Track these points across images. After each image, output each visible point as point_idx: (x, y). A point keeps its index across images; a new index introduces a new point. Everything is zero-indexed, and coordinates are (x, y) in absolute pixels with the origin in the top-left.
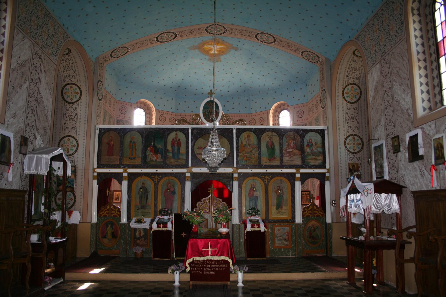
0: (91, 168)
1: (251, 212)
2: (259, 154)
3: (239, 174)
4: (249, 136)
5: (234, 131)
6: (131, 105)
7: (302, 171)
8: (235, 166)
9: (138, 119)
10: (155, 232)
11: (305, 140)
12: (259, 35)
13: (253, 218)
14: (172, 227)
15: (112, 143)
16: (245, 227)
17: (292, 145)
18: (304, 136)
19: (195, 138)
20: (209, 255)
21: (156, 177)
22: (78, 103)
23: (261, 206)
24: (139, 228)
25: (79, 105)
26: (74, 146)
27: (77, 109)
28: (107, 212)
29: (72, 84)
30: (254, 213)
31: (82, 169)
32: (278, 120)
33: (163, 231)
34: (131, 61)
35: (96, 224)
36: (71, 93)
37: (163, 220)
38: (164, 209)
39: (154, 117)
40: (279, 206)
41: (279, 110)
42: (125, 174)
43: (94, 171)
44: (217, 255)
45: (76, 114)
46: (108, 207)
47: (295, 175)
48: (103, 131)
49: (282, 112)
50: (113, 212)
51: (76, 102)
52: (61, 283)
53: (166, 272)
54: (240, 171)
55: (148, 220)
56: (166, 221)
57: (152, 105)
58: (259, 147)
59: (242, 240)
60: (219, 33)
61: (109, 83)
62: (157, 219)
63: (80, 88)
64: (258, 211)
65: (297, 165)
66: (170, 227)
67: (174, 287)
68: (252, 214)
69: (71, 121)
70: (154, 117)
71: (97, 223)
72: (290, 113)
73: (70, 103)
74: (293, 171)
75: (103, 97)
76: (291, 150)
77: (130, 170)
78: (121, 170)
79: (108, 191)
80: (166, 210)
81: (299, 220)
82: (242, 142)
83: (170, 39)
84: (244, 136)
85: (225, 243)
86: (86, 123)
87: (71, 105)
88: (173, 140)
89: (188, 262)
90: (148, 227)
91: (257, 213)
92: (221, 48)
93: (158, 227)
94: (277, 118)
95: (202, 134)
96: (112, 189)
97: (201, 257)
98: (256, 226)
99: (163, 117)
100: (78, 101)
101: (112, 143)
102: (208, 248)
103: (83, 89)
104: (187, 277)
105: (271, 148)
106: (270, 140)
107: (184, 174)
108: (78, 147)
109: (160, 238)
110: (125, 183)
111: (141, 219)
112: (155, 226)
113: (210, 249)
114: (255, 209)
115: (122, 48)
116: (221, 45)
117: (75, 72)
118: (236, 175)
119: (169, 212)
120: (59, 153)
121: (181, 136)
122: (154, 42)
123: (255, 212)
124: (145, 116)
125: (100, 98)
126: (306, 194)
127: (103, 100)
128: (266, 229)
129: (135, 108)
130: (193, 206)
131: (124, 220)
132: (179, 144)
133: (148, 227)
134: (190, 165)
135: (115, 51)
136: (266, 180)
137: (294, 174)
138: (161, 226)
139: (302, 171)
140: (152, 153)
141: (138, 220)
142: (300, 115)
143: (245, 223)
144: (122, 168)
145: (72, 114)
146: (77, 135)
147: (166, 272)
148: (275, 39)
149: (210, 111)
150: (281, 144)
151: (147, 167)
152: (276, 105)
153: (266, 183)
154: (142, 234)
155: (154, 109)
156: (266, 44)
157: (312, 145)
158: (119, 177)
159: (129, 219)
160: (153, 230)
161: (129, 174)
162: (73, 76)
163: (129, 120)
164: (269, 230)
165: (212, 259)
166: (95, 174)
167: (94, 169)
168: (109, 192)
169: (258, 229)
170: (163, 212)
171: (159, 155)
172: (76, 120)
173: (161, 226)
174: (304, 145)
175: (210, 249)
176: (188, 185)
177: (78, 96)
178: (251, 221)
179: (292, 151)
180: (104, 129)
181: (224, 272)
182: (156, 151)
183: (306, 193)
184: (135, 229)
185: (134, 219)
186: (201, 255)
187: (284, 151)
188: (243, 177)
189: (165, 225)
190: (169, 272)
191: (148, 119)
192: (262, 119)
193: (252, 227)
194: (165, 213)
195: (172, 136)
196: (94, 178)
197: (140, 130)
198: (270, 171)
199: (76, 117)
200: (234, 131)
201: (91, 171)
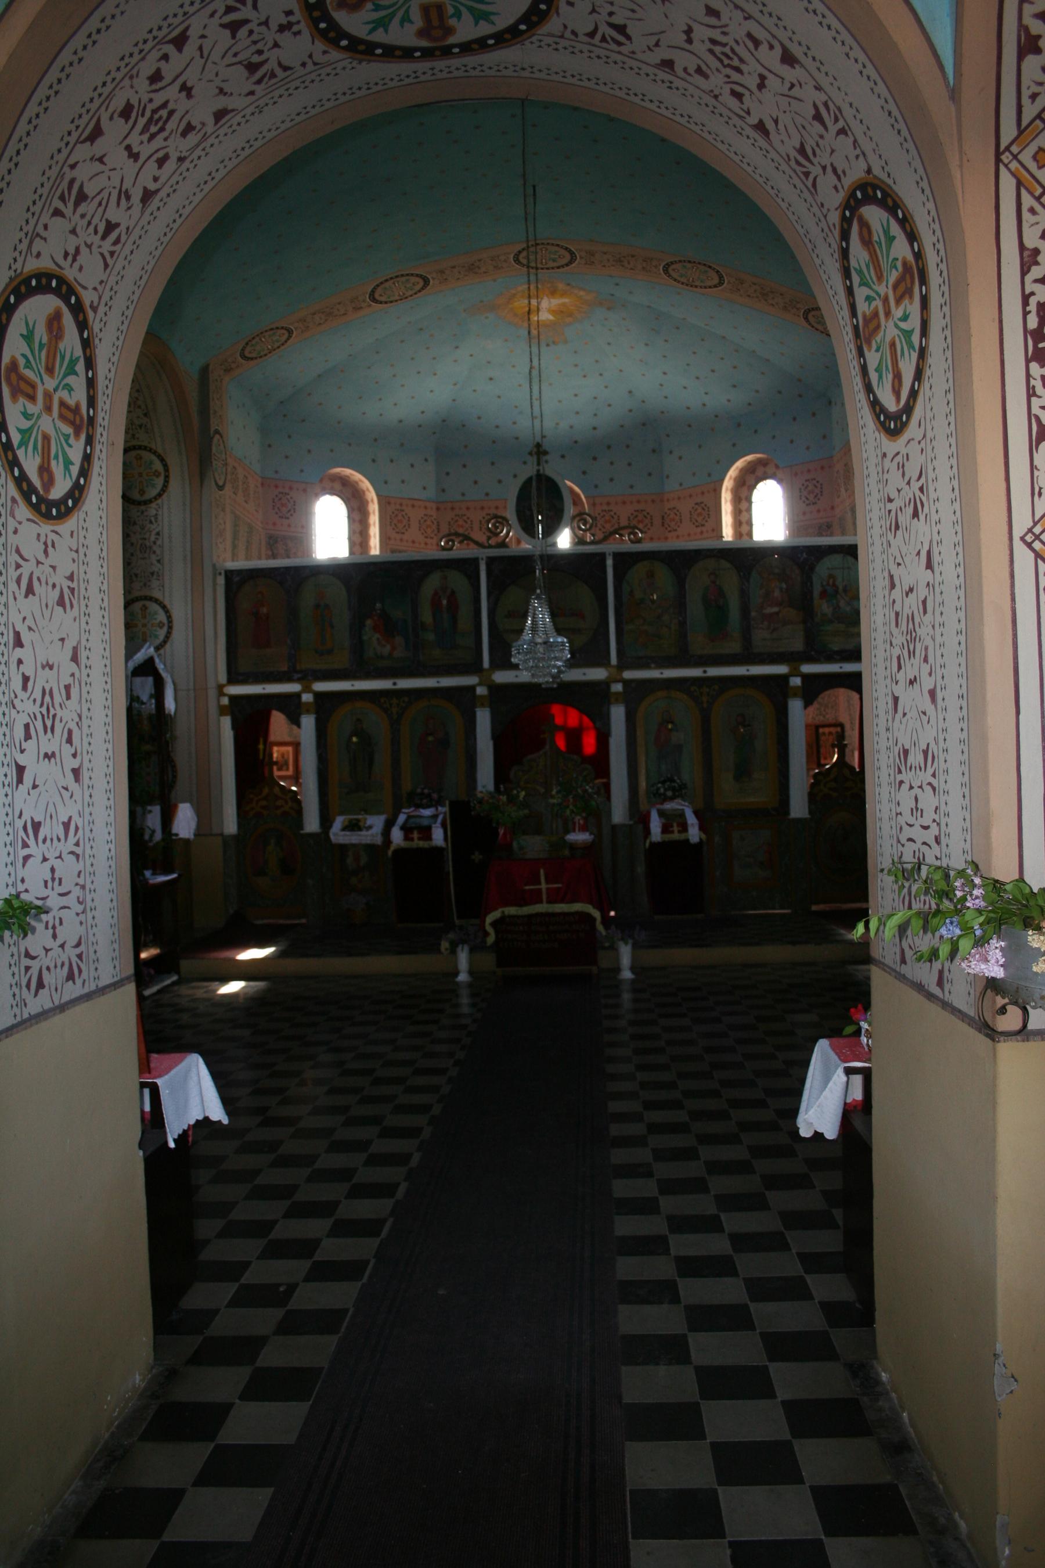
0: (212, 684)
1: (662, 790)
2: (682, 624)
3: (626, 683)
4: (651, 575)
5: (610, 562)
6: (305, 490)
7: (807, 668)
8: (614, 661)
9: (329, 532)
10: (399, 852)
11: (815, 579)
12: (673, 266)
13: (668, 806)
14: (446, 839)
15: (264, 610)
16: (647, 832)
17: (777, 593)
18: (812, 569)
19: (497, 588)
20: (541, 902)
21: (395, 701)
22: (159, 501)
23: (690, 771)
24: (354, 845)
25: (165, 507)
26: (161, 625)
27: (160, 518)
28: (264, 803)
29: (140, 448)
30: (669, 793)
31: (188, 690)
32: (749, 510)
33: (419, 850)
34: (300, 363)
35: (236, 838)
36: (140, 475)
37: (418, 820)
38: (419, 790)
39: (374, 520)
40: (742, 772)
41: (744, 493)
42: (307, 698)
43: (221, 694)
44: (562, 901)
45: (158, 534)
46: (266, 791)
47: (788, 682)
48: (236, 579)
49: (761, 486)
50: (279, 803)
51: (155, 498)
52: (174, 984)
53: (435, 949)
54: (628, 675)
55: (376, 822)
56: (425, 822)
57: (366, 484)
58: (680, 603)
59: (641, 869)
60: (555, 264)
61: (239, 434)
62: (402, 818)
63: (162, 460)
64: (683, 786)
65: (792, 653)
66: (438, 836)
67: (457, 984)
68: (664, 794)
69: (146, 555)
70: (374, 520)
71: (239, 834)
72: (785, 489)
73: (139, 503)
74: (782, 669)
75: (229, 477)
76: (775, 609)
77: (321, 686)
78: (293, 687)
79: (261, 747)
80: (426, 791)
81: (799, 807)
82: (631, 593)
83: (410, 293)
84: (638, 573)
85: (580, 872)
86: (189, 558)
87: (143, 508)
88: (436, 593)
89: (490, 918)
90: (379, 840)
91: (679, 792)
92: (564, 305)
93: (407, 838)
94: (744, 505)
95: (513, 574)
96: (272, 738)
97: (521, 906)
98: (675, 828)
99: (400, 517)
100: (160, 495)
101: (264, 610)
102: (540, 883)
103: (172, 461)
104: (488, 961)
105: (716, 606)
106: (714, 582)
107: (472, 688)
108: (170, 628)
109: (413, 866)
110: (308, 722)
111: (358, 820)
112: (397, 836)
113: (544, 886)
114: (674, 781)
115: (271, 332)
116: (562, 295)
117: (145, 415)
118: (617, 688)
119: (435, 796)
120: (146, 657)
121: (458, 581)
122: (363, 305)
123: (674, 789)
124: (349, 517)
125: (221, 483)
126: (830, 733)
127: (228, 486)
128: (704, 837)
129: (317, 496)
130: (501, 775)
131: (312, 824)
132: (453, 606)
133: (379, 840)
134: (486, 664)
135: (254, 342)
136: (705, 699)
137: (784, 679)
138: (415, 835)
139: (807, 668)
140: (377, 636)
141: (350, 821)
142: (811, 497)
143: (645, 820)
144: (298, 680)
145: (147, 536)
146: (167, 594)
147: (435, 949)
148: (721, 277)
149: (541, 501)
150: (744, 594)
151: (368, 676)
152: (740, 464)
153: (705, 705)
154: (364, 860)
155: (372, 495)
156: (699, 290)
157: (837, 592)
158: (291, 707)
159: (326, 821)
160: (392, 848)
161: (319, 696)
162: (141, 426)
163: (302, 537)
164: (717, 839)
165: (550, 910)
166: (225, 701)
167: (220, 688)
168: (265, 750)
169: (682, 837)
170: (417, 800)
171: (399, 640)
172: (158, 552)
173: (415, 835)
174: (811, 593)
175: (544, 886)
176: (483, 719)
177: (159, 482)
178: (661, 814)
179: (777, 613)
180: (240, 572)
181: (581, 944)
182: (388, 628)
183: (833, 730)
184: (343, 848)
185: (339, 822)
186: (522, 902)
187: (753, 614)
188: (636, 692)
189: (426, 832)
190: (443, 949)
191: (357, 517)
192: (700, 510)
193: (666, 829)
194: (425, 801)
195: (432, 583)
196: (223, 711)
197: (335, 570)
198: (714, 672)
199: (159, 542)
200: (610, 562)
201: (212, 693)
